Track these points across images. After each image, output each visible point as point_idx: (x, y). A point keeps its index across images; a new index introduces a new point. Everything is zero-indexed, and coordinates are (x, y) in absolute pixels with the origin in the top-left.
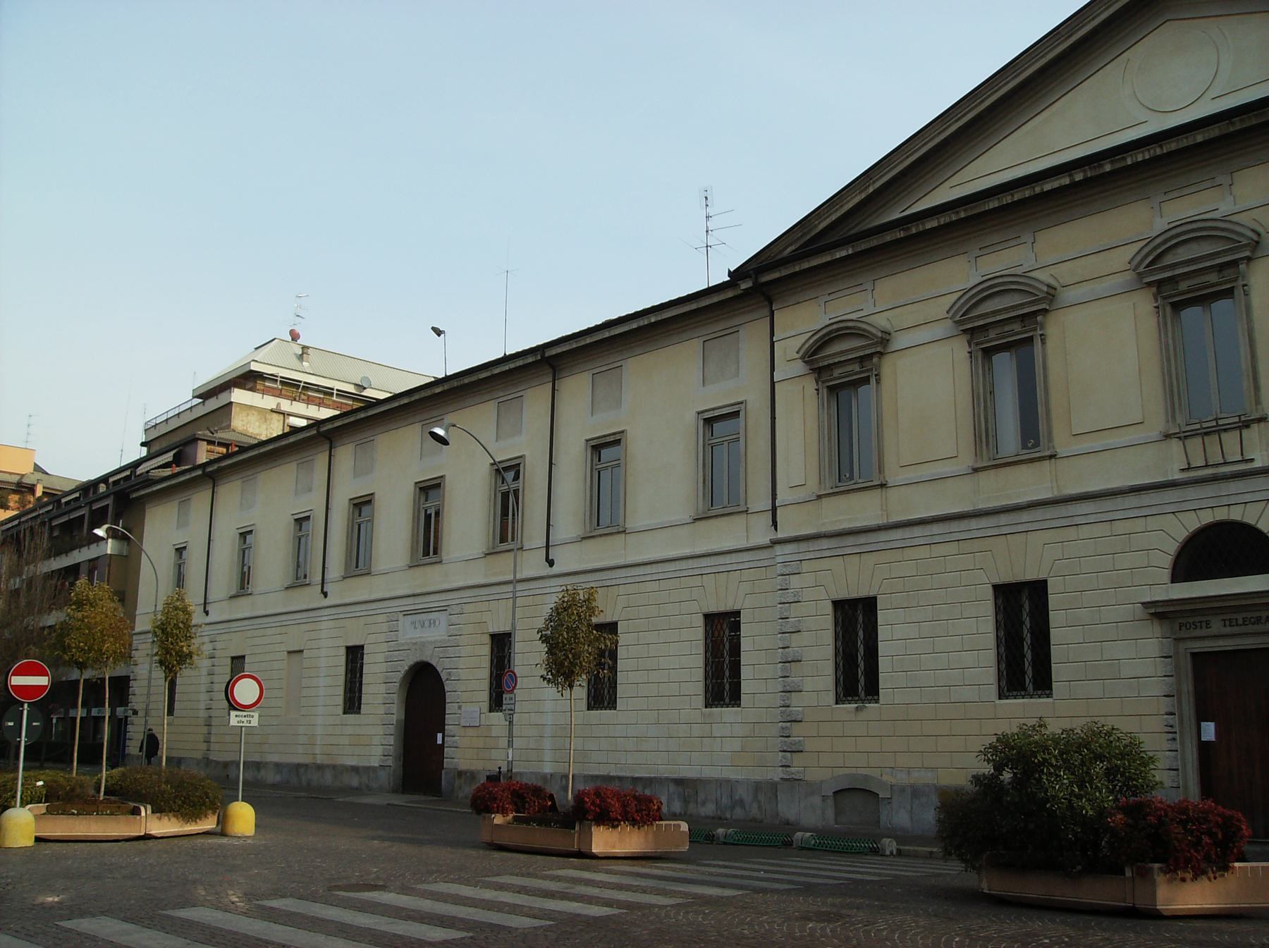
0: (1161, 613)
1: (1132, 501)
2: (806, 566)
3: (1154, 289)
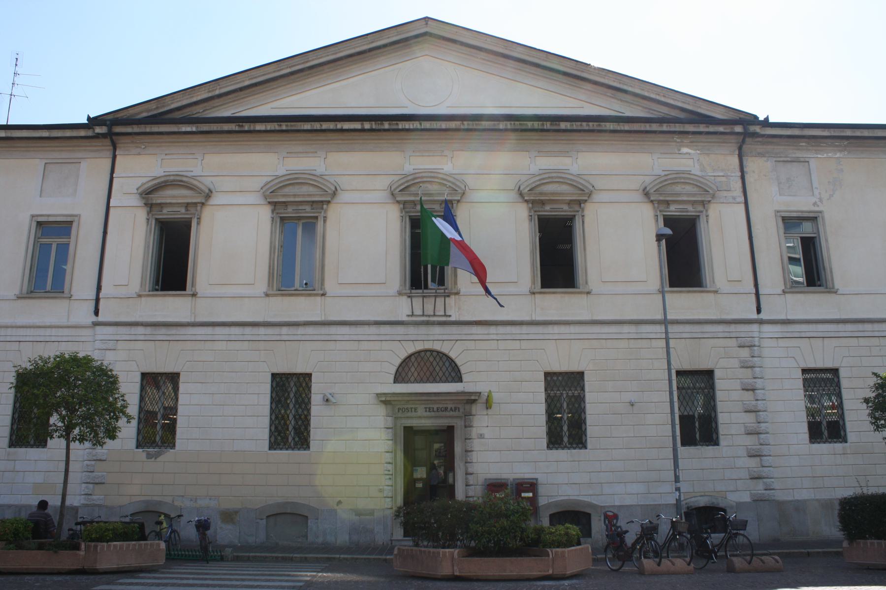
0: (386, 400)
1: (373, 330)
2: (121, 345)
3: (402, 206)
